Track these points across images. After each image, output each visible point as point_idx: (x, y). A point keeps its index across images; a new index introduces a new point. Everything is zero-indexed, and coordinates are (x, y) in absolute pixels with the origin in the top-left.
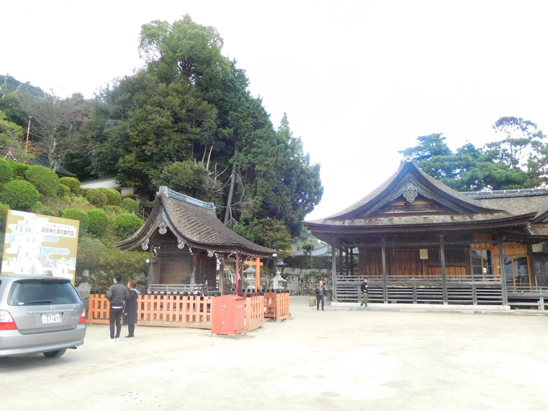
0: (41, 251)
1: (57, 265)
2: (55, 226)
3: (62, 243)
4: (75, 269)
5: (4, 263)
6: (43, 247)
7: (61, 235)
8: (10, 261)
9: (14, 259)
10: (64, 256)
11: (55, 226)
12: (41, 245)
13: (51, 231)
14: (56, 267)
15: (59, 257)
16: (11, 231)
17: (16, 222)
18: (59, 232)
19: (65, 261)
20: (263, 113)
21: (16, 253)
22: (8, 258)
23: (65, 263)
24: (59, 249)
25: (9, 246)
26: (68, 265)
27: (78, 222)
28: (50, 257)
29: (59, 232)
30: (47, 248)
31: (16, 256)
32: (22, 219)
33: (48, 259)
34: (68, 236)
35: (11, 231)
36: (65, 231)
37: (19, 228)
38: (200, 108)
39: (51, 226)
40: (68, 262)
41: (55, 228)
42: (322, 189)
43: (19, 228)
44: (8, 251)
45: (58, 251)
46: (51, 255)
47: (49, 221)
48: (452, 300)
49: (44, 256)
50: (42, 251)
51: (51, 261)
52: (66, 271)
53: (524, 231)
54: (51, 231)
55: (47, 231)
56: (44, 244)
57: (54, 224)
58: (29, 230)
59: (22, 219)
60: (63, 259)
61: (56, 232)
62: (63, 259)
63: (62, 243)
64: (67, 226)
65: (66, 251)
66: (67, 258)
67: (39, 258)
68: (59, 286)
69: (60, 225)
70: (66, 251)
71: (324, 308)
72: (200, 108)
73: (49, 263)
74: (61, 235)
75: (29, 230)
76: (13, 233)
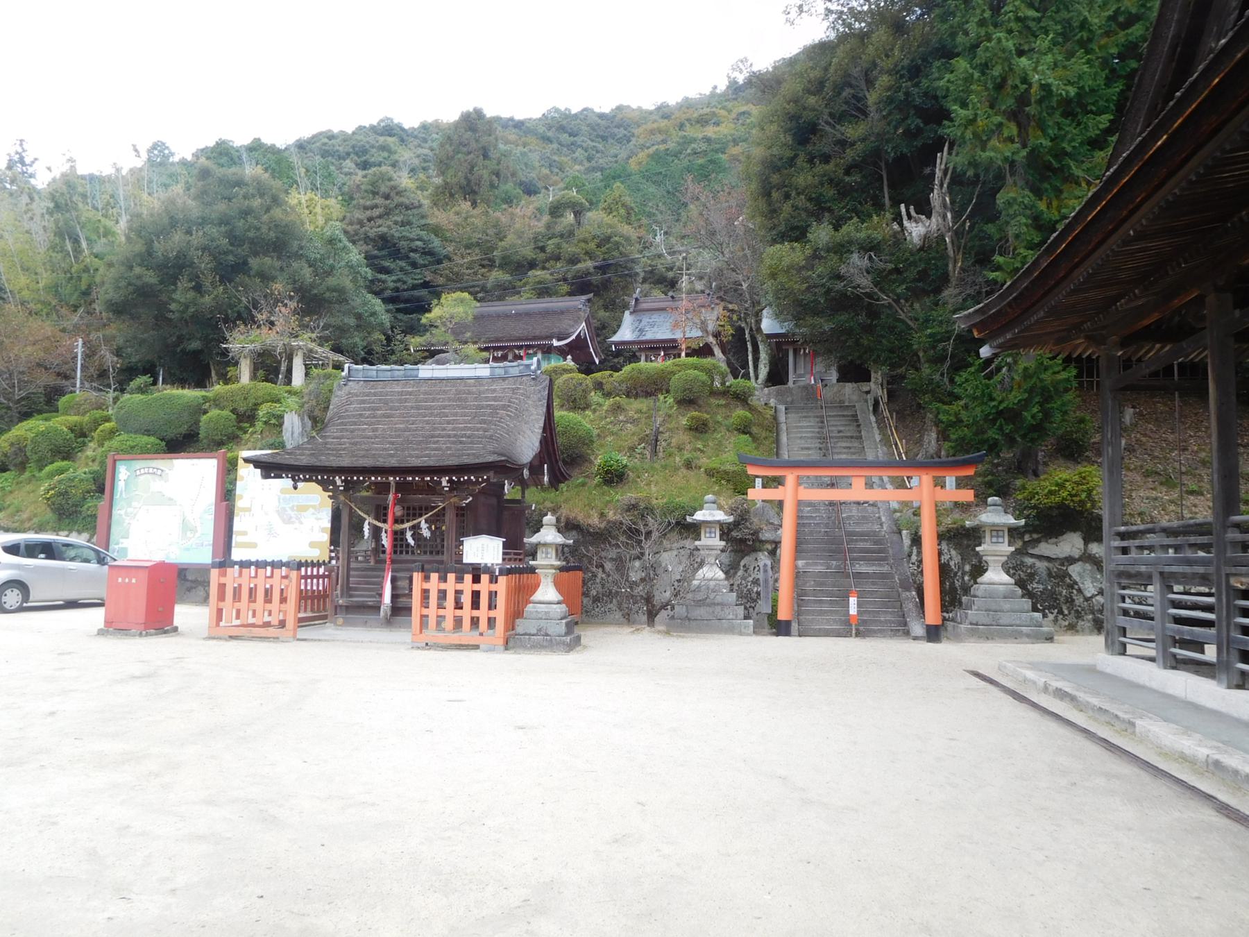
28: (292, 509)
33: (289, 512)
51: (292, 514)
60: (311, 510)
62: (311, 510)
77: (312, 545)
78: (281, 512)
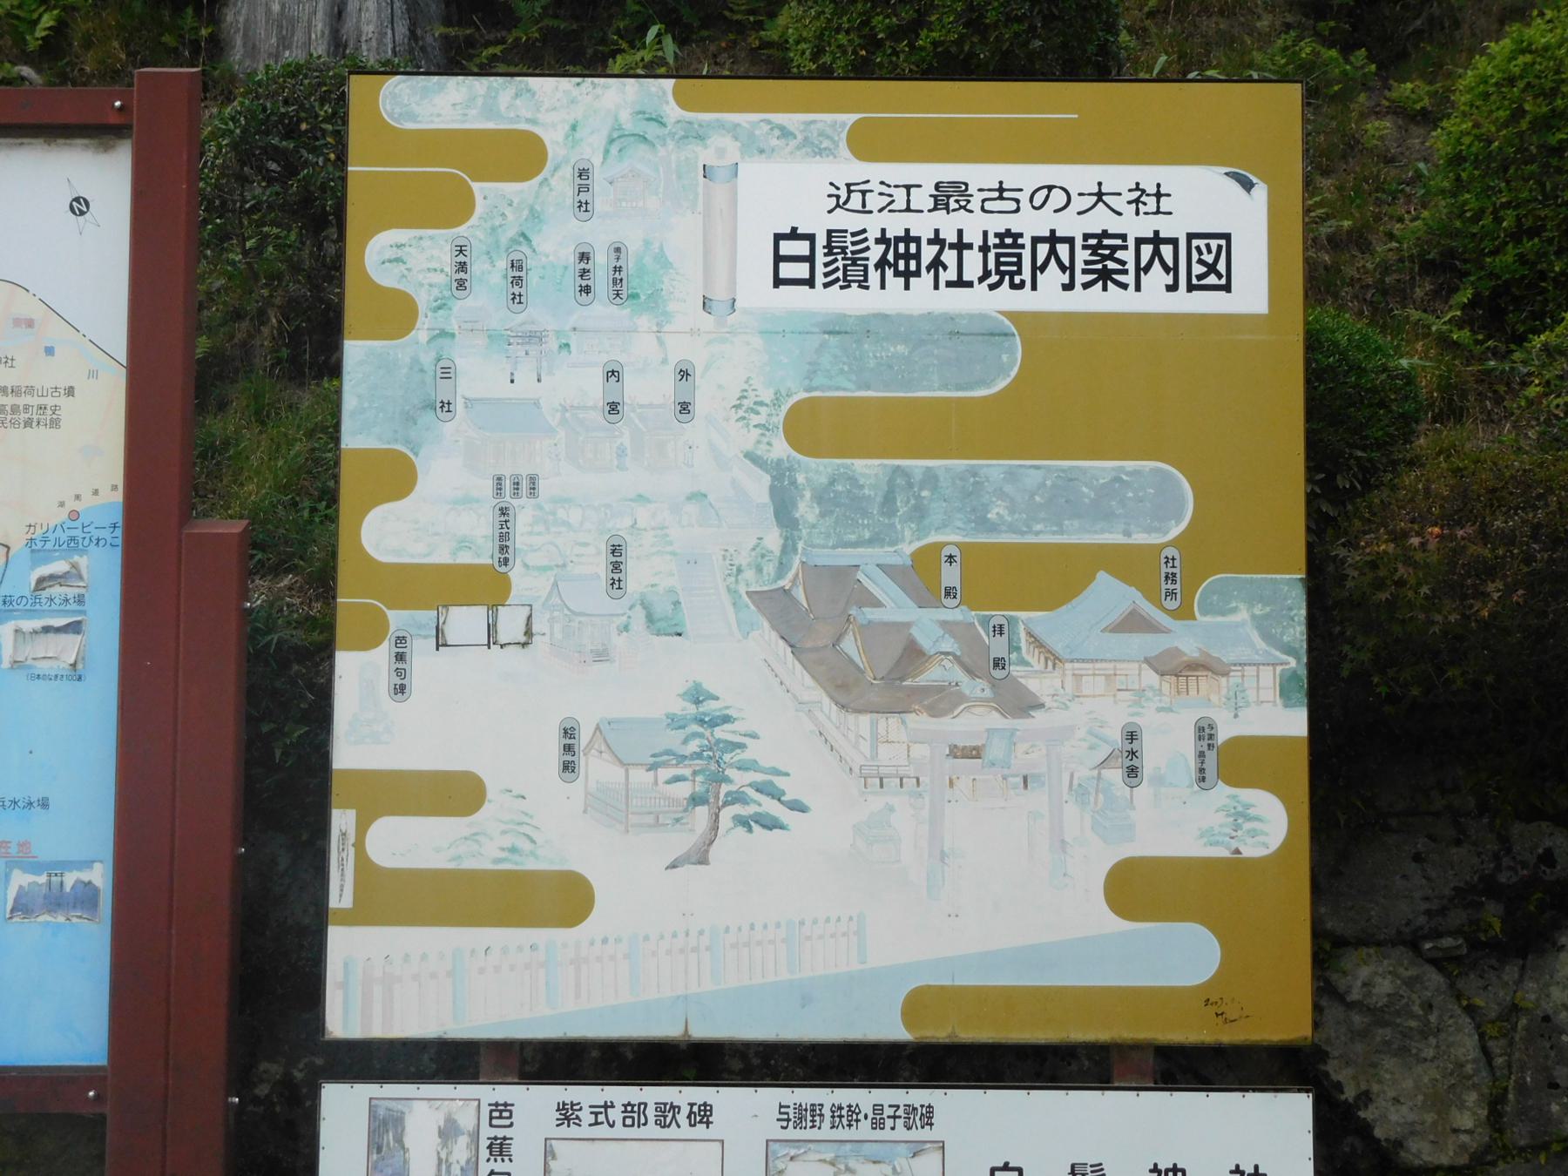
0: (784, 513)
1: (1036, 680)
2: (947, 196)
3: (1070, 396)
4: (1295, 723)
5: (356, 675)
6: (815, 470)
7: (1049, 295)
8: (422, 655)
9: (466, 621)
10: (1127, 563)
12: (780, 449)
13: (902, 257)
14: (1021, 704)
15: (1053, 576)
16: (397, 314)
17: (451, 208)
18: (1007, 260)
19: (1132, 623)
21: (484, 555)
22: (397, 619)
23: (1153, 644)
24: (1036, 472)
25: (397, 477)
28: (921, 576)
29: (1007, 260)
30: (868, 469)
31: (485, 586)
32: (519, 155)
34: (1154, 296)
35: (397, 314)
36: (1102, 245)
37: (490, 274)
38: (731, 37)
39: (899, 193)
40: (1186, 640)
43: (490, 274)
44: (383, 534)
45: (1018, 497)
46: (927, 560)
47: (865, 145)
49: (843, 576)
50: (806, 510)
51: (928, 626)
52: (1170, 745)
54: (902, 257)
55: (844, 261)
56: (814, 426)
58: (609, 278)
59: (519, 155)
60: (1109, 594)
61: (973, 264)
62: (1109, 594)
63: (1070, 396)
65: (1150, 500)
66: (1171, 579)
67: (776, 606)
68: (966, 659)
69: (1024, 176)
70: (1150, 500)
72: (731, 37)
73: (913, 655)
74: (1049, 295)
75: (609, 278)
76: (421, 334)
77: (1138, 889)
78: (808, 616)
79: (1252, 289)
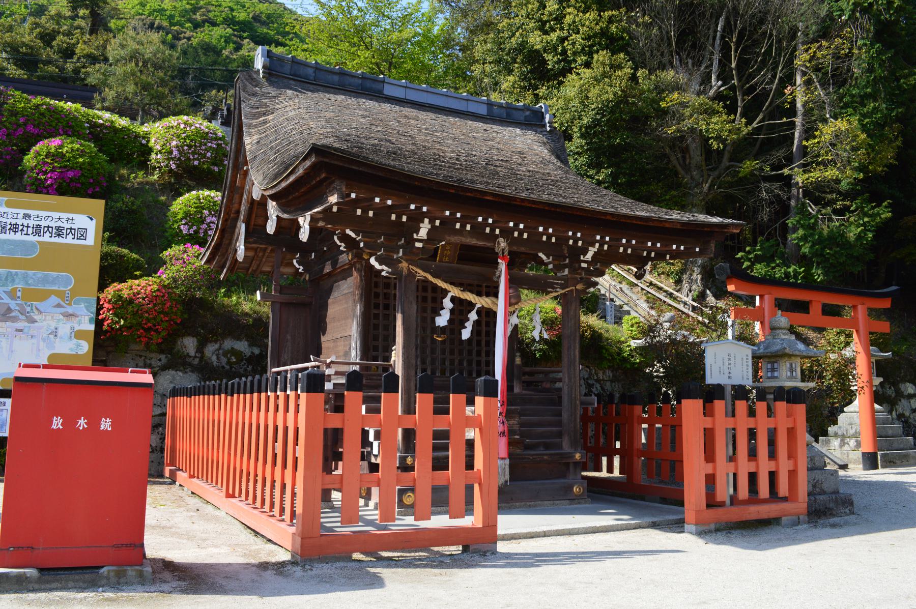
7: (46, 238)
10: (60, 294)
11: (25, 217)
15: (43, 296)
18: (38, 230)
19: (59, 306)
20: (514, 422)
26: (68, 316)
27: (101, 203)
29: (38, 230)
34: (69, 240)
41: (26, 222)
42: (376, 582)
47: (9, 204)
48: (508, 386)
53: (523, 382)
57: (22, 212)
60: (54, 300)
62: (54, 300)
64: (64, 216)
65: (65, 281)
69: (43, 214)
71: (42, 310)
73: (9, 310)
74: (46, 238)
79: (91, 240)
